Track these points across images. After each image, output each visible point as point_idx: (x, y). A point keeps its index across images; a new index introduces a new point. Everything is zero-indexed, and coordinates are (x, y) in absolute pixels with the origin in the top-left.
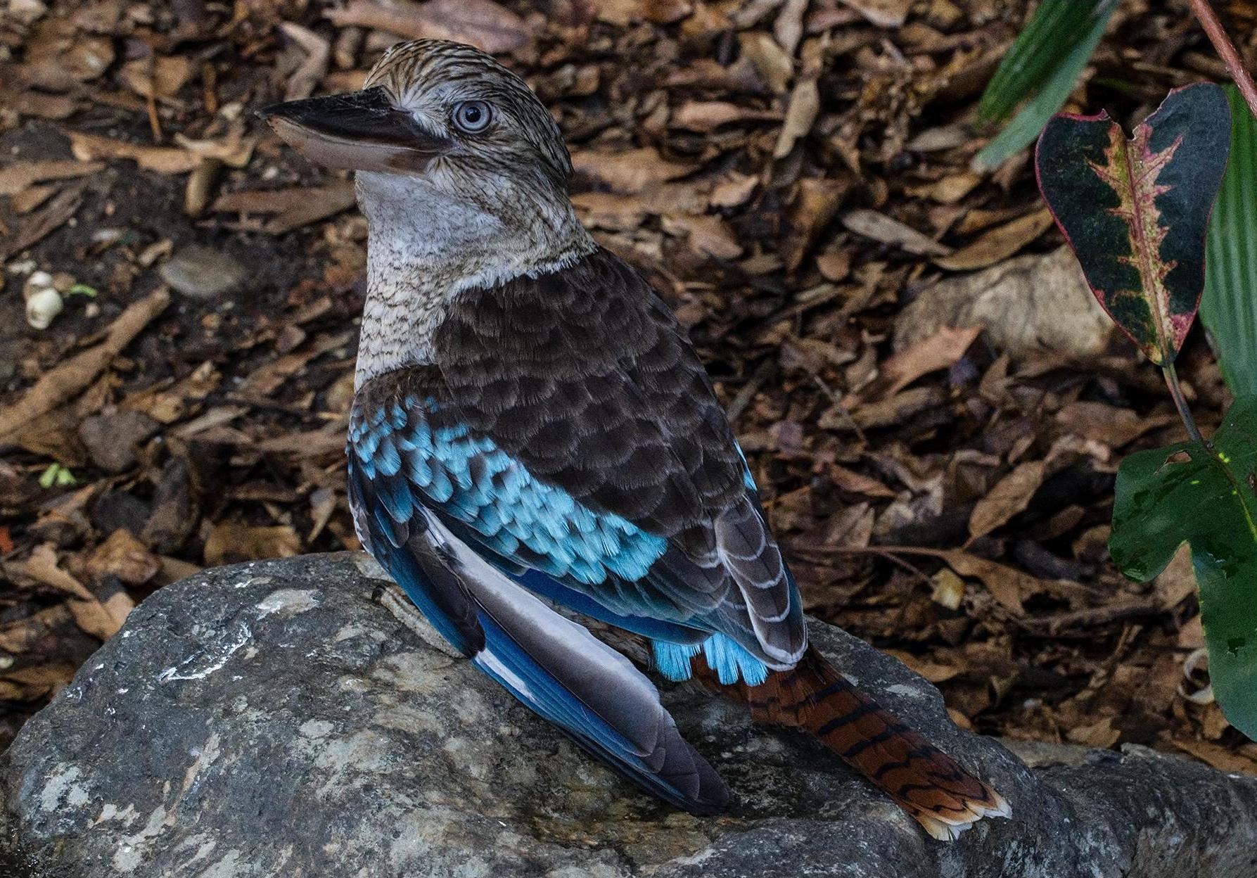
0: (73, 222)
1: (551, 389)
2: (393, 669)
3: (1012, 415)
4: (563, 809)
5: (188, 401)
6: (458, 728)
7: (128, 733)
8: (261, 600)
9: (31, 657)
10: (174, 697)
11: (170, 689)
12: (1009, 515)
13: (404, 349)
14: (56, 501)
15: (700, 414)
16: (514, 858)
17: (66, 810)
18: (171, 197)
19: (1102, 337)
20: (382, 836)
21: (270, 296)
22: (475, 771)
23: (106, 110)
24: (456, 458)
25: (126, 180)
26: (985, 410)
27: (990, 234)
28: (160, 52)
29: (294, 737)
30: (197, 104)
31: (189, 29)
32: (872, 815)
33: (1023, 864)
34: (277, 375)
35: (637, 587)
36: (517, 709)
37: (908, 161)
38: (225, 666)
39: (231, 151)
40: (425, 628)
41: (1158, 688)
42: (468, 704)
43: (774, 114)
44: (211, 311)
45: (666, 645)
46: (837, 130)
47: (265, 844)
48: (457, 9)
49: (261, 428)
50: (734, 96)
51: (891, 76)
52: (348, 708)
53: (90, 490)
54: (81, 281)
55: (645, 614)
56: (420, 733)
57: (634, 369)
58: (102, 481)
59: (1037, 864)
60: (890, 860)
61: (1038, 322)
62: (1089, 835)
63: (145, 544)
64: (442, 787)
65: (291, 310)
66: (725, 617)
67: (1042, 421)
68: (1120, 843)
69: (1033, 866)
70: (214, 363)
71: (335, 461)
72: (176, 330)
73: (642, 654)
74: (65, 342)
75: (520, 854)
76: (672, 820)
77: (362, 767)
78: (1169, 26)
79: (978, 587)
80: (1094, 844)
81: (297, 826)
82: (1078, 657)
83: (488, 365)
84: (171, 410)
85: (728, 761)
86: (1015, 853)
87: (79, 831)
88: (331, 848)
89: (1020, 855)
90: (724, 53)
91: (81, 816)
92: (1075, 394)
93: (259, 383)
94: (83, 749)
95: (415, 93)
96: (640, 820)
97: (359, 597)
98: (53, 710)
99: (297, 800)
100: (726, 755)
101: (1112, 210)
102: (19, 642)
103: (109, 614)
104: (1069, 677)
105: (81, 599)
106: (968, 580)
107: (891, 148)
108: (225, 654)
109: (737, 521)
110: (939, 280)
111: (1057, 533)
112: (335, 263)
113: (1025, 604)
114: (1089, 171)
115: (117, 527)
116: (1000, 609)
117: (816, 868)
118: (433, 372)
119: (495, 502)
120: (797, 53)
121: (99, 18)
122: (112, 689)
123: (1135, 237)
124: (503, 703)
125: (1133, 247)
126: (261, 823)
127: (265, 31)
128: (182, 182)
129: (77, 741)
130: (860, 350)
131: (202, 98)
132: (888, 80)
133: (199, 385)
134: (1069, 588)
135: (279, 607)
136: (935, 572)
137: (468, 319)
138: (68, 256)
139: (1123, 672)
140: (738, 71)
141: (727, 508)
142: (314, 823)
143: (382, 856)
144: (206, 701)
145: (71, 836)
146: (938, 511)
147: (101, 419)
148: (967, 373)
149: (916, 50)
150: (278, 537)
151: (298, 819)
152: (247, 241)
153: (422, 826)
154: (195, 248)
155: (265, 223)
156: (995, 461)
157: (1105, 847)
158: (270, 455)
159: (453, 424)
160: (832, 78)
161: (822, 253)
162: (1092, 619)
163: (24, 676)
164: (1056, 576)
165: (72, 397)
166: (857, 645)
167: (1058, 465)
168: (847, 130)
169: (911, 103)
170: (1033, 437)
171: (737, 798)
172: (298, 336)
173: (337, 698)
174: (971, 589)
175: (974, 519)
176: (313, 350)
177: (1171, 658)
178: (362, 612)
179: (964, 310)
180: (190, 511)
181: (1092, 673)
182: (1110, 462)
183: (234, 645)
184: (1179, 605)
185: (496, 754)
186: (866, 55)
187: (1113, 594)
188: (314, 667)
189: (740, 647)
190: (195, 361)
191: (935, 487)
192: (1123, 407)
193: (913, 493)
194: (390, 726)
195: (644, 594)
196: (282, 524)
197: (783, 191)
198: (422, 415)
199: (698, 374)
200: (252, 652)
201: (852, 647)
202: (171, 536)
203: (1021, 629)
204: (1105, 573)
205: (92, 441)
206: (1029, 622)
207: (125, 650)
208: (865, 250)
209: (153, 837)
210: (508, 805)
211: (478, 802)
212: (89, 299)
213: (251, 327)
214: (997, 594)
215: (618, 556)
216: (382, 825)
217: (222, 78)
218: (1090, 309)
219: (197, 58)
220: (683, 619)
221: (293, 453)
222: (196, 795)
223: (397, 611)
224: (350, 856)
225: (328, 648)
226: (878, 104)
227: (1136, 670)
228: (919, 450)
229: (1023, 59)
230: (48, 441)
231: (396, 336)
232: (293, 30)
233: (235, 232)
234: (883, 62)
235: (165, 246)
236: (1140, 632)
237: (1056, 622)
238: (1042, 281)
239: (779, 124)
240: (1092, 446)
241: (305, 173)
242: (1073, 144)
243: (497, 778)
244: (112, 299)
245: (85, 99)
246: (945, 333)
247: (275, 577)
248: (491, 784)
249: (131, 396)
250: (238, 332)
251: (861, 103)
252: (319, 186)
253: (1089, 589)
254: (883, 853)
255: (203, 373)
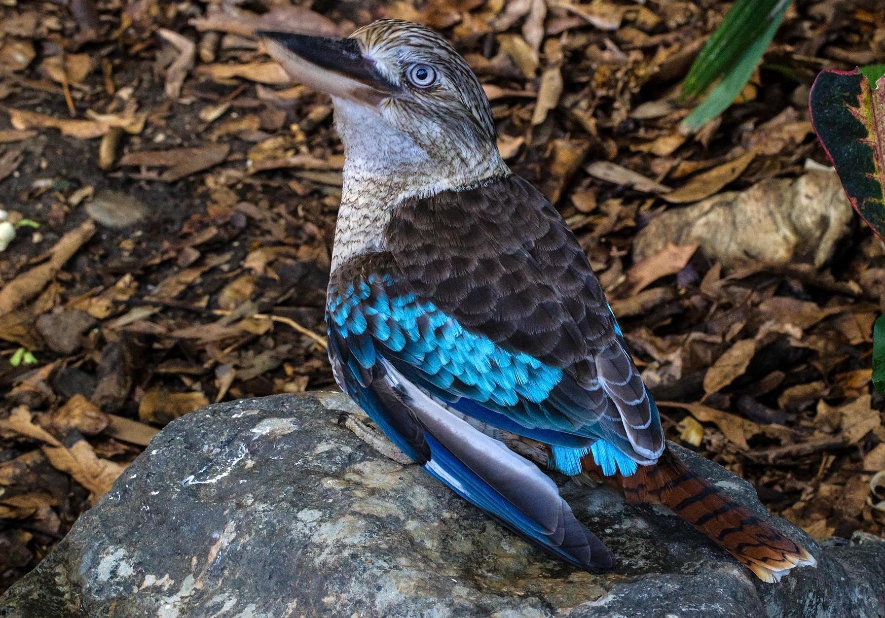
0: (17, 174)
1: (474, 265)
2: (359, 473)
3: (726, 307)
4: (495, 570)
5: (116, 303)
6: (413, 514)
7: (161, 523)
8: (254, 426)
9: (16, 488)
10: (196, 496)
11: (192, 491)
12: (732, 377)
13: (367, 239)
14: (26, 375)
15: (582, 281)
16: (467, 604)
17: (117, 580)
18: (88, 155)
19: (788, 250)
20: (367, 590)
21: (169, 226)
22: (428, 544)
23: (32, 94)
24: (407, 318)
25: (53, 143)
26: (705, 303)
27: (699, 177)
28: (69, 51)
29: (294, 522)
30: (99, 89)
31: (89, 34)
32: (720, 570)
33: (816, 610)
34: (180, 283)
35: (540, 406)
36: (454, 500)
37: (631, 126)
38: (231, 474)
39: (130, 122)
40: (380, 444)
41: (851, 500)
42: (418, 497)
43: (529, 92)
44: (126, 237)
45: (563, 449)
46: (575, 104)
47: (275, 599)
48: (288, 19)
49: (171, 322)
50: (498, 80)
51: (615, 66)
52: (331, 501)
53: (50, 367)
54: (26, 216)
55: (547, 427)
56: (387, 517)
57: (533, 249)
58: (59, 361)
59: (825, 610)
60: (738, 602)
61: (739, 240)
62: (857, 590)
63: (97, 405)
64: (407, 554)
65: (186, 236)
66: (605, 428)
67: (751, 310)
68: (877, 596)
69: (822, 612)
70: (133, 275)
71: (228, 345)
72: (101, 252)
73: (543, 457)
74: (19, 261)
75: (471, 601)
76: (575, 577)
77: (348, 541)
78: (812, 28)
79: (713, 430)
80: (860, 596)
81: (300, 585)
82: (791, 479)
83: (428, 249)
84: (104, 309)
85: (610, 535)
86: (811, 602)
87: (127, 595)
88: (328, 600)
89: (814, 603)
90: (487, 51)
91: (128, 584)
92: (771, 291)
93: (168, 289)
94: (126, 536)
95: (381, 48)
96: (550, 578)
97: (328, 423)
98: (100, 509)
99: (300, 566)
100: (608, 531)
101: (862, 139)
102: (7, 477)
103: (75, 457)
104: (784, 493)
105: (52, 446)
106: (706, 425)
107: (618, 117)
108: (230, 465)
109: (612, 358)
110: (666, 210)
111: (767, 391)
112: (215, 202)
113: (749, 442)
114: (847, 112)
115: (73, 394)
116: (730, 444)
117: (690, 607)
118: (387, 257)
119: (437, 349)
120: (541, 49)
121: (21, 26)
122: (145, 492)
123: (877, 159)
124: (444, 496)
125: (876, 167)
126: (272, 584)
127: (146, 35)
128: (94, 144)
129: (121, 531)
130: (609, 262)
131: (103, 84)
132: (614, 67)
133: (123, 291)
134: (779, 430)
135: (268, 431)
136: (681, 419)
137: (410, 218)
138: (16, 198)
139: (825, 489)
140: (498, 62)
141: (603, 348)
142: (313, 583)
143: (369, 605)
144: (221, 498)
145: (121, 599)
146: (678, 376)
147: (53, 316)
148: (691, 276)
149: (630, 46)
150: (193, 400)
151: (300, 580)
152: (147, 188)
153: (398, 582)
154: (109, 192)
155: (160, 174)
156: (718, 339)
157: (868, 599)
158: (182, 340)
159: (405, 293)
160: (569, 67)
161: (573, 193)
162: (799, 452)
163: (16, 501)
164: (768, 422)
165: (31, 300)
166: (690, 454)
167: (766, 342)
168: (584, 104)
169: (632, 84)
170: (744, 322)
171: (620, 562)
172: (194, 255)
173: (321, 494)
174: (708, 432)
175: (707, 381)
176: (205, 265)
177: (859, 478)
178: (332, 433)
179: (685, 232)
180: (126, 382)
181: (802, 490)
182: (802, 339)
183: (235, 459)
184: (860, 441)
185: (443, 532)
186: (593, 50)
187: (812, 434)
188: (302, 472)
189: (617, 450)
190: (118, 274)
191: (676, 358)
192: (806, 300)
193: (659, 362)
194: (365, 513)
195: (545, 411)
196: (194, 391)
197: (541, 149)
198: (381, 288)
199: (578, 252)
200: (250, 463)
201: (686, 456)
202: (115, 400)
203: (746, 458)
204: (804, 419)
205: (47, 332)
206: (753, 454)
207: (153, 464)
208: (605, 190)
209: (187, 597)
210: (455, 568)
211: (434, 566)
212: (34, 230)
213: (157, 250)
214: (727, 434)
215: (527, 384)
216: (368, 582)
217: (116, 70)
218: (777, 230)
219: (97, 54)
220: (575, 429)
221: (197, 339)
222: (219, 565)
223: (358, 431)
224: (343, 605)
225: (310, 459)
226: (608, 84)
227: (834, 487)
228: (660, 332)
229: (717, 50)
230: (15, 332)
231: (362, 229)
232: (166, 34)
233: (138, 181)
234: (606, 55)
235: (88, 190)
236: (835, 461)
237: (772, 454)
238: (741, 210)
239: (534, 100)
240: (789, 328)
241: (186, 137)
242: (836, 91)
243: (445, 549)
244: (51, 230)
245: (16, 85)
246: (672, 248)
247: (261, 410)
248: (441, 553)
249: (72, 300)
250: (147, 253)
251: (594, 84)
252: (196, 146)
253: (792, 430)
254: (734, 597)
255: (125, 283)
